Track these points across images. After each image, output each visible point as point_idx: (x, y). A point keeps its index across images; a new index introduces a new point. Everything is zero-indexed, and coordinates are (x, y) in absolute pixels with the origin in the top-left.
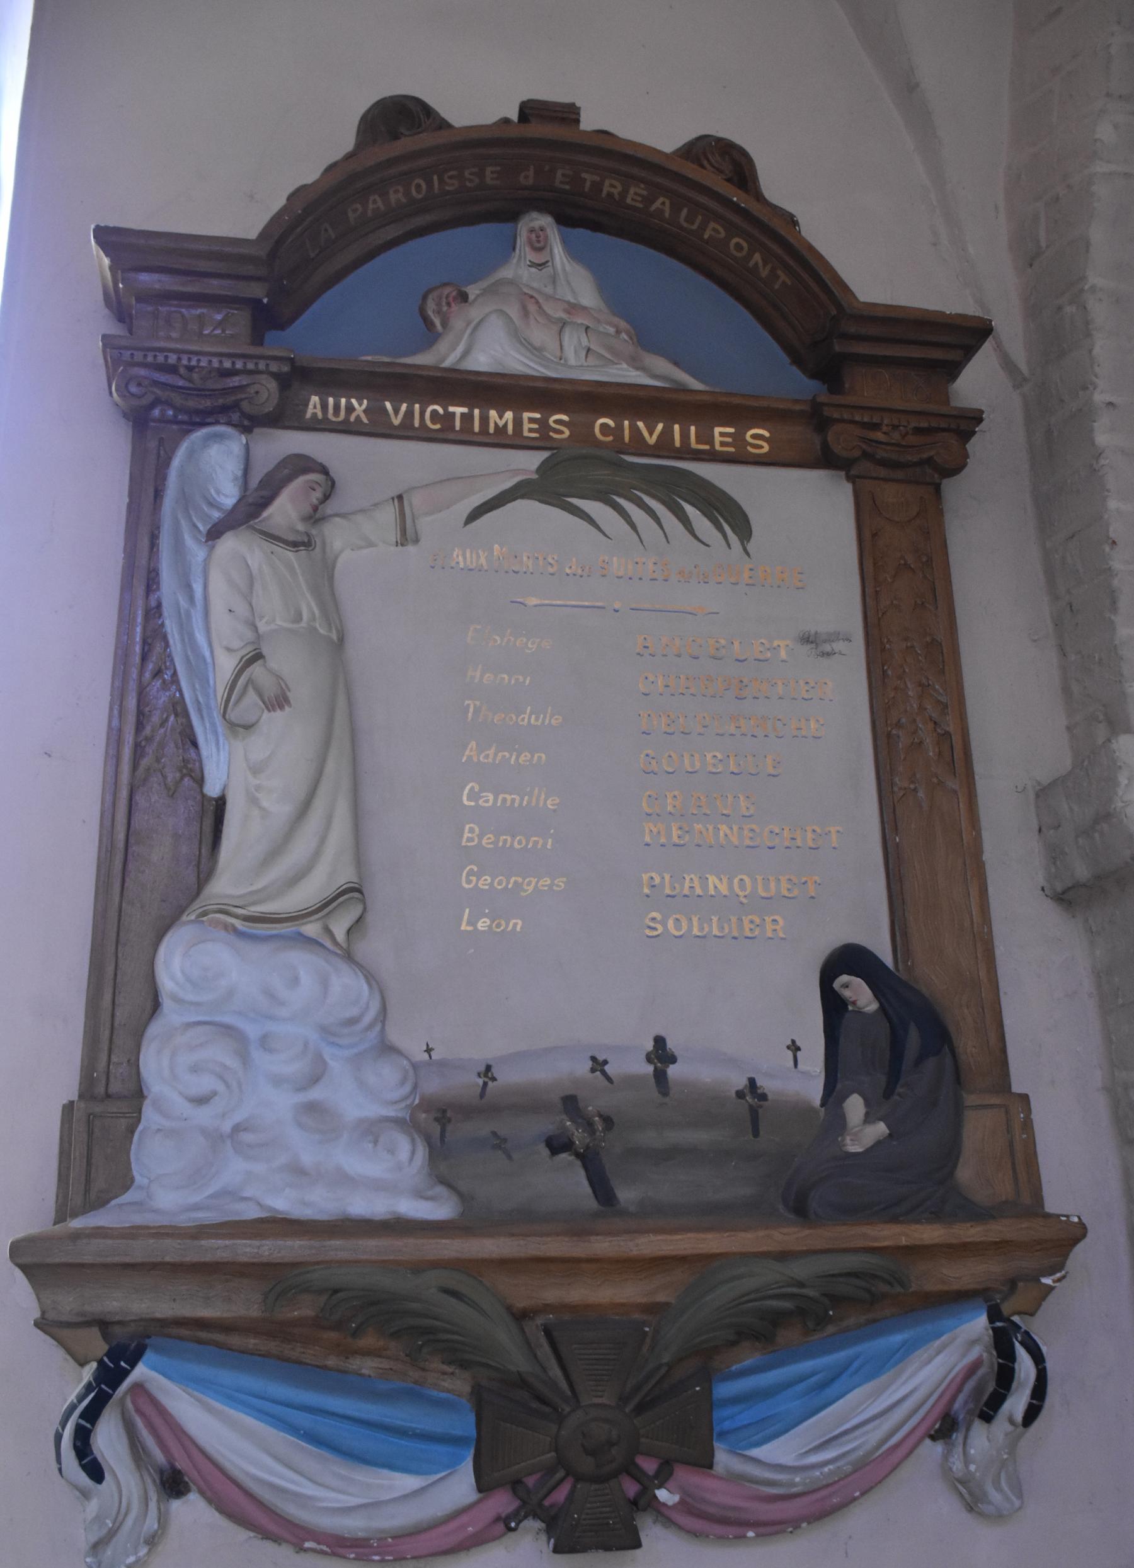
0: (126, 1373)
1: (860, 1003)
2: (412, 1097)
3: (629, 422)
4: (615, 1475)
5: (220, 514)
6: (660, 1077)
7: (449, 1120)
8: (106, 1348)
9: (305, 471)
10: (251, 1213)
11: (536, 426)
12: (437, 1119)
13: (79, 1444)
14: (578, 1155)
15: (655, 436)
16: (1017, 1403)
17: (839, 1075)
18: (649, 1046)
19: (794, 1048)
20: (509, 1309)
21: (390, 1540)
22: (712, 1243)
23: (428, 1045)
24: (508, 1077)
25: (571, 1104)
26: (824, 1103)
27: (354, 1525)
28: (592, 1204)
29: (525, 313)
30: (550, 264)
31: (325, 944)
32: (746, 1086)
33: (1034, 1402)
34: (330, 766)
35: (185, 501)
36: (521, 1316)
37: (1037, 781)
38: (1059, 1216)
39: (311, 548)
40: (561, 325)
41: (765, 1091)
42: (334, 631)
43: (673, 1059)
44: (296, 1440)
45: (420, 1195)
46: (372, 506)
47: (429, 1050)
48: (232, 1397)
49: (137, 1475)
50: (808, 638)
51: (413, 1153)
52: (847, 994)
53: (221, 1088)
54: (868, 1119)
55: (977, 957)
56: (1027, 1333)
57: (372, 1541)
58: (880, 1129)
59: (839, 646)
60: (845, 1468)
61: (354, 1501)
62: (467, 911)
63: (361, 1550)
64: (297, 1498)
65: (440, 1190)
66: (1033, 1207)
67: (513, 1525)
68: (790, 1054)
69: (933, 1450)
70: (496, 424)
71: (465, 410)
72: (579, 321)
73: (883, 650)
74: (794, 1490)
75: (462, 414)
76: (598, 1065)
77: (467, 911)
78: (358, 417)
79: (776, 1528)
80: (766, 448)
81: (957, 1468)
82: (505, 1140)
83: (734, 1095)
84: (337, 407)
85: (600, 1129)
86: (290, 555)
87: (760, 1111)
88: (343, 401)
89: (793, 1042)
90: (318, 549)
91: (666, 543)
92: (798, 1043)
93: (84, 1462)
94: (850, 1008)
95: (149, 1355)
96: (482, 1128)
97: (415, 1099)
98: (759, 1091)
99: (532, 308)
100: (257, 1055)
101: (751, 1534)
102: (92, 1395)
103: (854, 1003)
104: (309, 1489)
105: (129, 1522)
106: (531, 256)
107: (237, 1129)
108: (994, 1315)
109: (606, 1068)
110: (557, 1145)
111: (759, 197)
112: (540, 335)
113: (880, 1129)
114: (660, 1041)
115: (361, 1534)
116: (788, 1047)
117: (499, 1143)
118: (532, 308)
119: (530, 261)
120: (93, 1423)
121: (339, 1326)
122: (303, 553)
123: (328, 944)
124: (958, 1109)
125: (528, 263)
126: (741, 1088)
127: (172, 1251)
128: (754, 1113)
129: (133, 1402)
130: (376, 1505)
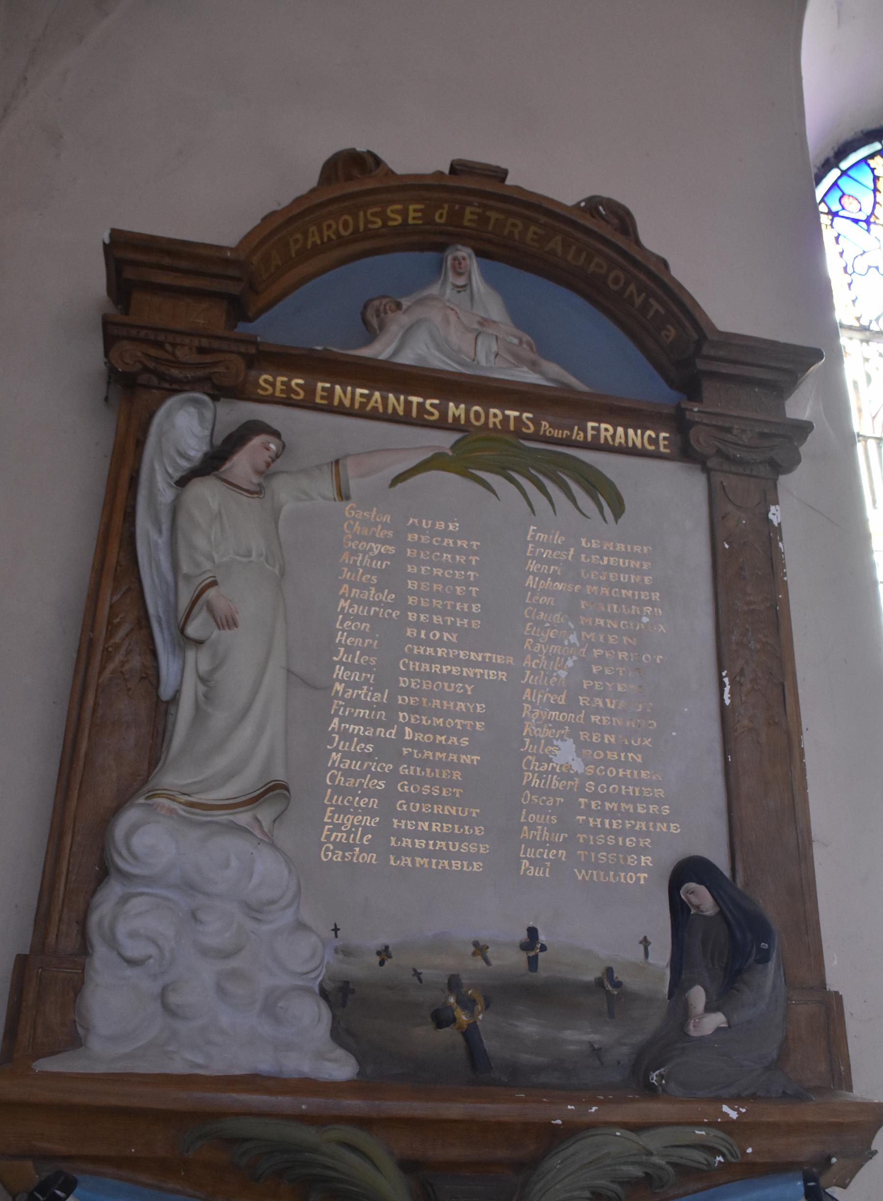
1: (703, 908)
3: (466, 406)
19: (645, 942)
23: (335, 925)
29: (446, 321)
30: (468, 287)
31: (253, 832)
39: (262, 496)
40: (475, 334)
52: (694, 899)
54: (709, 1008)
65: (340, 1052)
71: (517, 414)
75: (515, 417)
103: (698, 907)
111: (637, 242)
114: (532, 932)
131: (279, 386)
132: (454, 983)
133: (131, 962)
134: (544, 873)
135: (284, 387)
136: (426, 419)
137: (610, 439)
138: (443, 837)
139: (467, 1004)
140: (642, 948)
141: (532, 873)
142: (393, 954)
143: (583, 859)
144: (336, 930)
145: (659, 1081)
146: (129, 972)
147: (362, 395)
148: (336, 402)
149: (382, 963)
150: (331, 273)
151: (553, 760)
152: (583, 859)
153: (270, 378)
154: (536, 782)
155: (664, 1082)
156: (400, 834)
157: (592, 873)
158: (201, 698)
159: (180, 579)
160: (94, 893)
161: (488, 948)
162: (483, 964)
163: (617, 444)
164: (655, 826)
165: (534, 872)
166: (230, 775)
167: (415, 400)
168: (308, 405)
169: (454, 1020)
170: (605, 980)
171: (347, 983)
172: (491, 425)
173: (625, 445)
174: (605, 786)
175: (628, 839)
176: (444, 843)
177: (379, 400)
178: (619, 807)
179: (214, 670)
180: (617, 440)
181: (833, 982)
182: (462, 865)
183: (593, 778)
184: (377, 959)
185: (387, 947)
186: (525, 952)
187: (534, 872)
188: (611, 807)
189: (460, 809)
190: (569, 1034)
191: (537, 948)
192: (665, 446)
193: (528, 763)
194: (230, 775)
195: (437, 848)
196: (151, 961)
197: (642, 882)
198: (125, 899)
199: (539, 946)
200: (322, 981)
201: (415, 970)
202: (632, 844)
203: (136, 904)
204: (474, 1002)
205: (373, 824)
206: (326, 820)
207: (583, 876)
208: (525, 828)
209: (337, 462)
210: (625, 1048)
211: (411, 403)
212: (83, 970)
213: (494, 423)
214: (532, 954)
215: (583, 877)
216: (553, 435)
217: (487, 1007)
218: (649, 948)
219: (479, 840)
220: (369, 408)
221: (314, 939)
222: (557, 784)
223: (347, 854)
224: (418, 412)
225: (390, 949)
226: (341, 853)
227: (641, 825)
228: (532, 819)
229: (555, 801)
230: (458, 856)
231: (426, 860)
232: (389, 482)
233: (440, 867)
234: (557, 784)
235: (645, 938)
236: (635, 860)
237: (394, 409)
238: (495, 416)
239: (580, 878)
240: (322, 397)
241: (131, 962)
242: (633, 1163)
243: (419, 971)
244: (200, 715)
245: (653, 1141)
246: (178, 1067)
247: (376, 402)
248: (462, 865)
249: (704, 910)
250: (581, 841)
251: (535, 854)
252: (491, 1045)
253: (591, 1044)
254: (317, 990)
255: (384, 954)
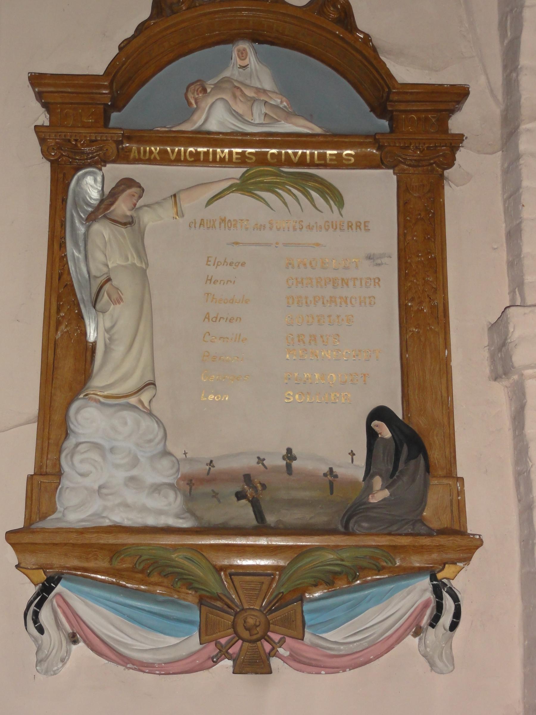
0: (53, 588)
4: (259, 640)
5: (91, 209)
6: (289, 467)
7: (194, 484)
8: (45, 577)
9: (130, 187)
10: (107, 523)
11: (239, 156)
12: (188, 484)
13: (34, 618)
14: (249, 501)
15: (297, 158)
16: (446, 619)
17: (372, 467)
18: (284, 452)
19: (352, 454)
20: (214, 567)
21: (163, 665)
22: (303, 542)
24: (220, 466)
25: (247, 478)
26: (364, 480)
27: (147, 657)
28: (254, 522)
30: (249, 66)
32: (328, 471)
33: (455, 620)
34: (141, 328)
35: (76, 204)
36: (219, 569)
37: (489, 322)
38: (474, 535)
41: (337, 474)
43: (295, 458)
45: (178, 516)
46: (162, 200)
47: (185, 454)
48: (97, 600)
49: (58, 632)
50: (370, 257)
52: (376, 429)
55: (443, 413)
56: (450, 588)
57: (155, 665)
58: (386, 493)
59: (385, 260)
60: (364, 644)
61: (148, 647)
63: (151, 669)
64: (125, 645)
65: (187, 515)
66: (462, 533)
67: (215, 660)
68: (350, 457)
69: (411, 641)
70: (220, 157)
73: (406, 262)
74: (342, 653)
76: (260, 460)
78: (155, 156)
79: (333, 670)
80: (353, 160)
81: (422, 650)
82: (218, 494)
83: (322, 475)
84: (145, 151)
85: (260, 489)
86: (123, 230)
87: (334, 483)
88: (148, 148)
89: (352, 451)
90: (136, 225)
91: (301, 211)
92: (354, 452)
93: (36, 626)
94: (380, 436)
95: (62, 581)
96: (208, 489)
97: (178, 475)
98: (334, 474)
99: (238, 93)
100: (109, 456)
101: (323, 672)
102: (40, 597)
104: (129, 641)
105: (54, 651)
106: (240, 62)
107: (100, 487)
108: (433, 578)
109: (264, 462)
110: (240, 496)
112: (240, 108)
113: (386, 493)
114: (289, 450)
115: (151, 661)
116: (349, 454)
117: (215, 495)
118: (238, 93)
119: (239, 65)
120: (40, 609)
121: (142, 572)
122: (129, 228)
124: (426, 485)
125: (239, 66)
126: (326, 472)
127: (73, 539)
128: (331, 484)
129: (57, 602)
130: (157, 649)
150: (90, 631)
159: (91, 279)
166: (124, 378)
179: (113, 327)
194: (124, 378)
209: (175, 196)
232: (206, 203)
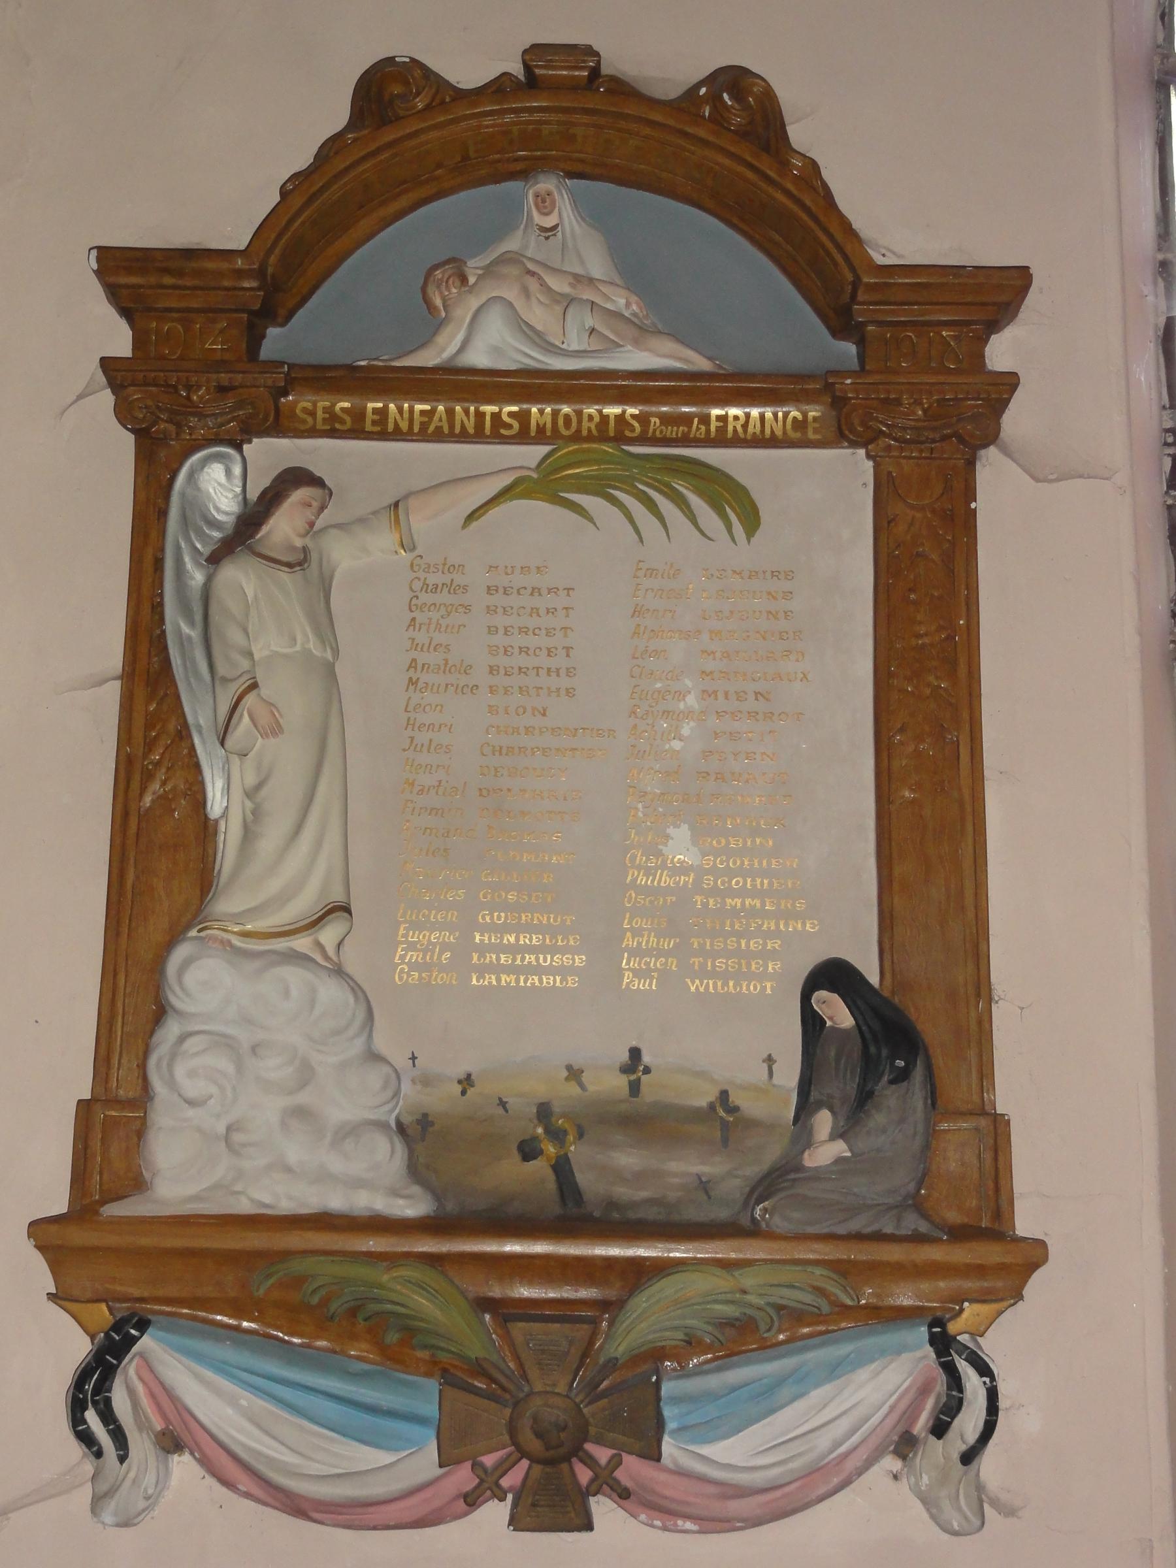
2: (394, 1102)
19: (770, 1060)
34: (322, 788)
42: (329, 650)
44: (274, 1409)
45: (395, 1193)
48: (221, 1368)
51: (393, 1152)
53: (214, 1090)
54: (833, 1137)
62: (108, 1357)
65: (416, 1189)
72: (585, 297)
75: (493, 414)
77: (108, 1357)
112: (539, 316)
114: (635, 1053)
123: (319, 958)
131: (320, 414)
132: (544, 1112)
133: (191, 1103)
134: (650, 985)
135: (327, 416)
136: (503, 434)
137: (739, 429)
138: (531, 949)
139: (557, 1135)
140: (765, 1066)
141: (636, 985)
142: (476, 1083)
143: (696, 967)
144: (413, 1058)
145: (763, 1216)
146: (191, 1113)
147: (422, 412)
148: (391, 427)
149: (464, 1093)
151: (663, 852)
152: (696, 967)
153: (309, 405)
154: (642, 879)
155: (767, 1216)
156: (482, 949)
157: (708, 983)
158: (250, 816)
159: (217, 683)
160: (152, 1033)
161: (583, 1072)
162: (578, 1090)
163: (749, 437)
164: (787, 925)
165: (639, 985)
167: (489, 409)
168: (357, 432)
169: (541, 1152)
170: (718, 1105)
171: (425, 1115)
172: (585, 433)
173: (761, 437)
174: (727, 880)
175: (752, 943)
176: (533, 957)
177: (444, 417)
178: (743, 904)
179: (259, 786)
180: (750, 429)
181: (1004, 1101)
182: (555, 981)
183: (713, 871)
184: (459, 1088)
185: (469, 1076)
186: (626, 1076)
187: (639, 985)
188: (733, 903)
189: (552, 916)
190: (674, 1166)
191: (640, 1071)
192: (816, 431)
193: (634, 857)
195: (525, 963)
196: (212, 1100)
197: (769, 991)
198: (182, 1039)
199: (641, 1068)
200: (399, 1115)
201: (500, 1099)
202: (758, 947)
203: (192, 1044)
204: (565, 1132)
205: (452, 940)
206: (400, 938)
207: (697, 986)
208: (629, 934)
209: (396, 505)
210: (739, 1180)
211: (483, 414)
212: (145, 1113)
213: (589, 430)
214: (633, 1077)
215: (697, 988)
216: (665, 435)
217: (581, 1135)
218: (775, 1067)
219: (575, 951)
220: (431, 428)
221: (386, 1069)
222: (668, 880)
223: (424, 975)
224: (492, 426)
225: (472, 1077)
226: (417, 974)
227: (769, 925)
228: (636, 924)
229: (665, 901)
230: (551, 971)
231: (513, 977)
233: (528, 984)
234: (668, 880)
235: (770, 1056)
236: (761, 966)
237: (463, 426)
238: (591, 417)
239: (693, 989)
240: (374, 423)
241: (191, 1103)
242: (727, 1302)
243: (504, 1100)
244: (249, 835)
245: (748, 1280)
246: (244, 1207)
247: (441, 420)
248: (555, 981)
249: (838, 1022)
250: (696, 945)
251: (639, 964)
252: (584, 1179)
253: (699, 1176)
254: (393, 1124)
255: (467, 1082)
